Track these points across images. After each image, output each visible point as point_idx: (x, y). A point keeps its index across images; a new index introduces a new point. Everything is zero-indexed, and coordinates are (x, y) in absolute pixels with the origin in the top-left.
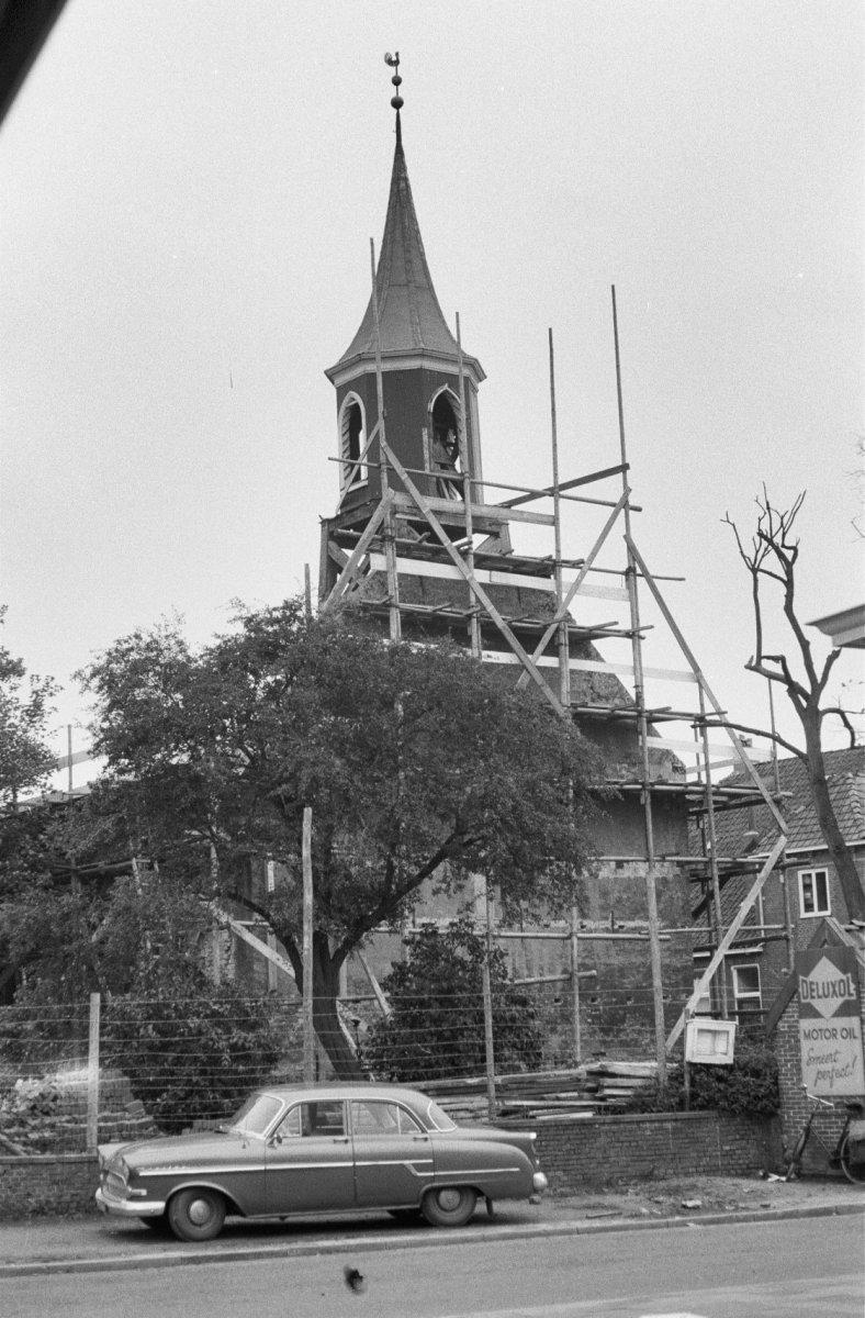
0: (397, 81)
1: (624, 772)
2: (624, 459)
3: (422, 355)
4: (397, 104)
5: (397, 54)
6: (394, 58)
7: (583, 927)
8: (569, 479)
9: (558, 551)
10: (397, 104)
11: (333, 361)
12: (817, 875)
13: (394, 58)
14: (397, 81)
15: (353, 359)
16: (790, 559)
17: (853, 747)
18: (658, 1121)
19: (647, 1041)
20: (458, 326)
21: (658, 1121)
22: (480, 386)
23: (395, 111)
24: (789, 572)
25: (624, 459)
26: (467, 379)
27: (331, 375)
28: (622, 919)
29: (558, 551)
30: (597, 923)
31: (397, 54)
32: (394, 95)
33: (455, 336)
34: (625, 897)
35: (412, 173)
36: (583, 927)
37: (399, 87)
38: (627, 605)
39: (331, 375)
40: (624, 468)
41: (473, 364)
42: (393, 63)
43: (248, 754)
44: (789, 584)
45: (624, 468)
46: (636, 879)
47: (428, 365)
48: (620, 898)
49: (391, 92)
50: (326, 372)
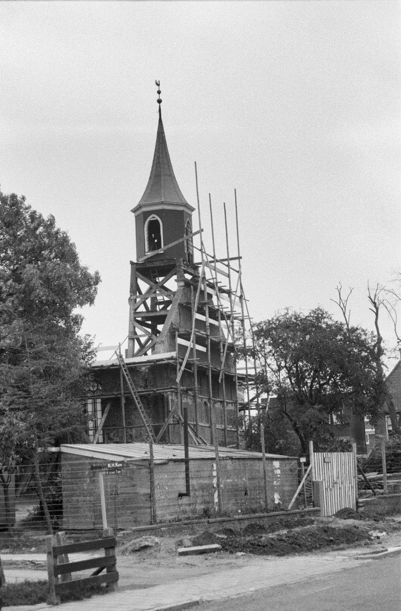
0: (159, 92)
2: (239, 255)
4: (159, 101)
8: (233, 257)
10: (159, 101)
11: (135, 205)
12: (238, 380)
14: (159, 92)
15: (139, 207)
18: (196, 419)
19: (9, 252)
21: (196, 419)
23: (158, 104)
24: (377, 310)
25: (239, 255)
27: (134, 211)
37: (161, 94)
38: (241, 309)
39: (134, 211)
40: (239, 258)
42: (158, 85)
43: (332, 418)
44: (377, 314)
45: (239, 258)
49: (157, 97)
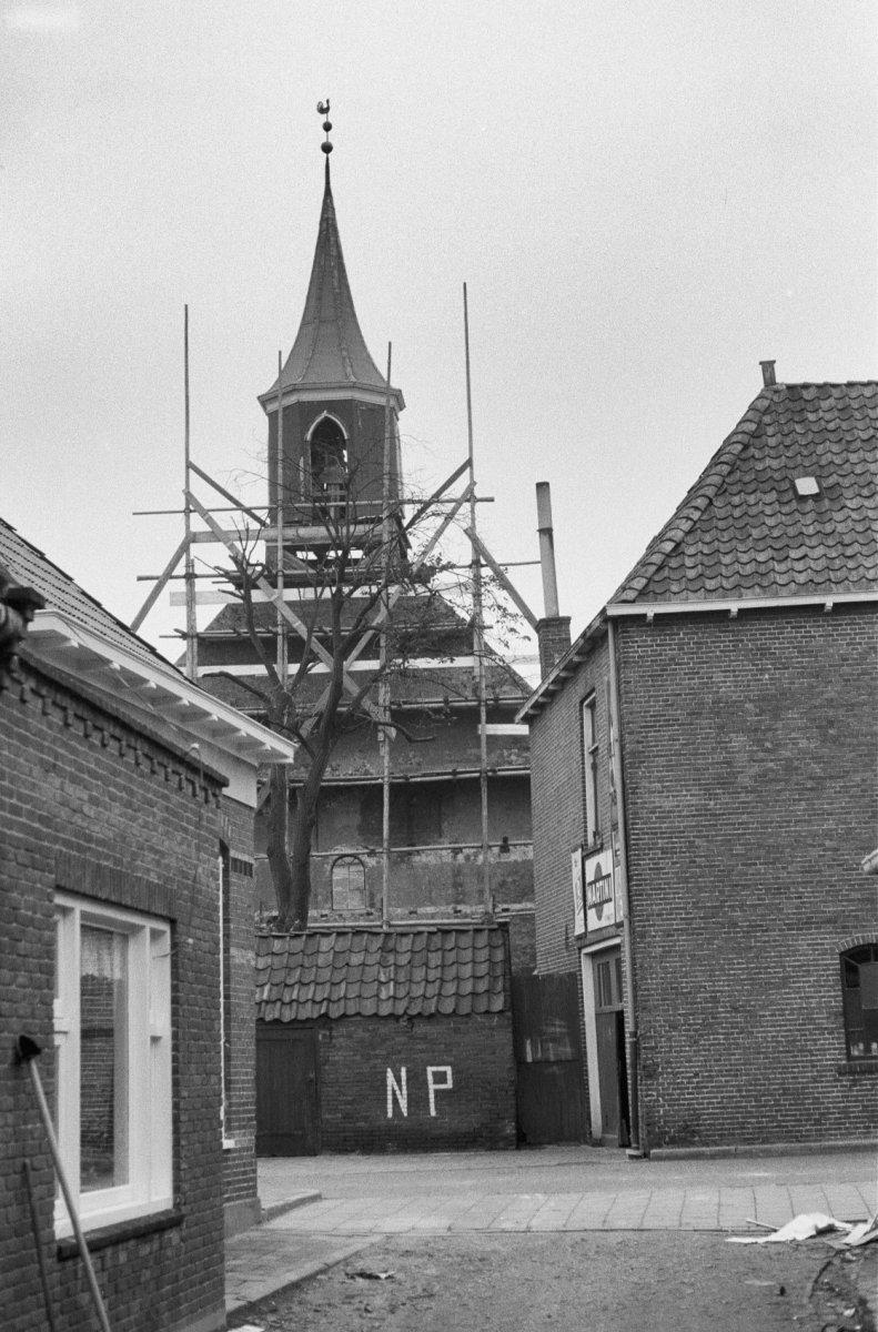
0: (327, 127)
1: (513, 758)
3: (353, 387)
4: (327, 148)
5: (328, 101)
6: (325, 106)
7: (456, 912)
9: (166, 956)
10: (327, 148)
13: (325, 106)
16: (175, 573)
17: (403, 502)
20: (389, 368)
22: (400, 414)
26: (393, 409)
27: (264, 401)
28: (505, 902)
29: (166, 956)
30: (474, 908)
31: (328, 101)
32: (324, 140)
33: (385, 377)
34: (510, 879)
35: (337, 203)
36: (456, 912)
39: (264, 401)
41: (398, 395)
46: (524, 862)
47: (358, 396)
48: (504, 881)
49: (322, 137)
50: (259, 398)
